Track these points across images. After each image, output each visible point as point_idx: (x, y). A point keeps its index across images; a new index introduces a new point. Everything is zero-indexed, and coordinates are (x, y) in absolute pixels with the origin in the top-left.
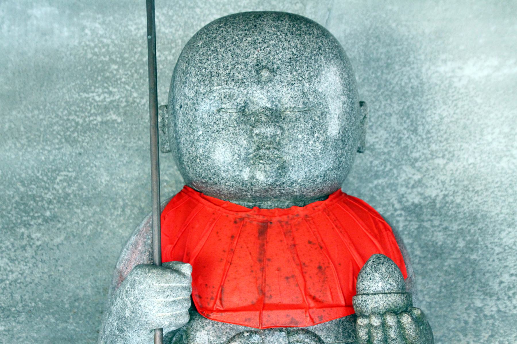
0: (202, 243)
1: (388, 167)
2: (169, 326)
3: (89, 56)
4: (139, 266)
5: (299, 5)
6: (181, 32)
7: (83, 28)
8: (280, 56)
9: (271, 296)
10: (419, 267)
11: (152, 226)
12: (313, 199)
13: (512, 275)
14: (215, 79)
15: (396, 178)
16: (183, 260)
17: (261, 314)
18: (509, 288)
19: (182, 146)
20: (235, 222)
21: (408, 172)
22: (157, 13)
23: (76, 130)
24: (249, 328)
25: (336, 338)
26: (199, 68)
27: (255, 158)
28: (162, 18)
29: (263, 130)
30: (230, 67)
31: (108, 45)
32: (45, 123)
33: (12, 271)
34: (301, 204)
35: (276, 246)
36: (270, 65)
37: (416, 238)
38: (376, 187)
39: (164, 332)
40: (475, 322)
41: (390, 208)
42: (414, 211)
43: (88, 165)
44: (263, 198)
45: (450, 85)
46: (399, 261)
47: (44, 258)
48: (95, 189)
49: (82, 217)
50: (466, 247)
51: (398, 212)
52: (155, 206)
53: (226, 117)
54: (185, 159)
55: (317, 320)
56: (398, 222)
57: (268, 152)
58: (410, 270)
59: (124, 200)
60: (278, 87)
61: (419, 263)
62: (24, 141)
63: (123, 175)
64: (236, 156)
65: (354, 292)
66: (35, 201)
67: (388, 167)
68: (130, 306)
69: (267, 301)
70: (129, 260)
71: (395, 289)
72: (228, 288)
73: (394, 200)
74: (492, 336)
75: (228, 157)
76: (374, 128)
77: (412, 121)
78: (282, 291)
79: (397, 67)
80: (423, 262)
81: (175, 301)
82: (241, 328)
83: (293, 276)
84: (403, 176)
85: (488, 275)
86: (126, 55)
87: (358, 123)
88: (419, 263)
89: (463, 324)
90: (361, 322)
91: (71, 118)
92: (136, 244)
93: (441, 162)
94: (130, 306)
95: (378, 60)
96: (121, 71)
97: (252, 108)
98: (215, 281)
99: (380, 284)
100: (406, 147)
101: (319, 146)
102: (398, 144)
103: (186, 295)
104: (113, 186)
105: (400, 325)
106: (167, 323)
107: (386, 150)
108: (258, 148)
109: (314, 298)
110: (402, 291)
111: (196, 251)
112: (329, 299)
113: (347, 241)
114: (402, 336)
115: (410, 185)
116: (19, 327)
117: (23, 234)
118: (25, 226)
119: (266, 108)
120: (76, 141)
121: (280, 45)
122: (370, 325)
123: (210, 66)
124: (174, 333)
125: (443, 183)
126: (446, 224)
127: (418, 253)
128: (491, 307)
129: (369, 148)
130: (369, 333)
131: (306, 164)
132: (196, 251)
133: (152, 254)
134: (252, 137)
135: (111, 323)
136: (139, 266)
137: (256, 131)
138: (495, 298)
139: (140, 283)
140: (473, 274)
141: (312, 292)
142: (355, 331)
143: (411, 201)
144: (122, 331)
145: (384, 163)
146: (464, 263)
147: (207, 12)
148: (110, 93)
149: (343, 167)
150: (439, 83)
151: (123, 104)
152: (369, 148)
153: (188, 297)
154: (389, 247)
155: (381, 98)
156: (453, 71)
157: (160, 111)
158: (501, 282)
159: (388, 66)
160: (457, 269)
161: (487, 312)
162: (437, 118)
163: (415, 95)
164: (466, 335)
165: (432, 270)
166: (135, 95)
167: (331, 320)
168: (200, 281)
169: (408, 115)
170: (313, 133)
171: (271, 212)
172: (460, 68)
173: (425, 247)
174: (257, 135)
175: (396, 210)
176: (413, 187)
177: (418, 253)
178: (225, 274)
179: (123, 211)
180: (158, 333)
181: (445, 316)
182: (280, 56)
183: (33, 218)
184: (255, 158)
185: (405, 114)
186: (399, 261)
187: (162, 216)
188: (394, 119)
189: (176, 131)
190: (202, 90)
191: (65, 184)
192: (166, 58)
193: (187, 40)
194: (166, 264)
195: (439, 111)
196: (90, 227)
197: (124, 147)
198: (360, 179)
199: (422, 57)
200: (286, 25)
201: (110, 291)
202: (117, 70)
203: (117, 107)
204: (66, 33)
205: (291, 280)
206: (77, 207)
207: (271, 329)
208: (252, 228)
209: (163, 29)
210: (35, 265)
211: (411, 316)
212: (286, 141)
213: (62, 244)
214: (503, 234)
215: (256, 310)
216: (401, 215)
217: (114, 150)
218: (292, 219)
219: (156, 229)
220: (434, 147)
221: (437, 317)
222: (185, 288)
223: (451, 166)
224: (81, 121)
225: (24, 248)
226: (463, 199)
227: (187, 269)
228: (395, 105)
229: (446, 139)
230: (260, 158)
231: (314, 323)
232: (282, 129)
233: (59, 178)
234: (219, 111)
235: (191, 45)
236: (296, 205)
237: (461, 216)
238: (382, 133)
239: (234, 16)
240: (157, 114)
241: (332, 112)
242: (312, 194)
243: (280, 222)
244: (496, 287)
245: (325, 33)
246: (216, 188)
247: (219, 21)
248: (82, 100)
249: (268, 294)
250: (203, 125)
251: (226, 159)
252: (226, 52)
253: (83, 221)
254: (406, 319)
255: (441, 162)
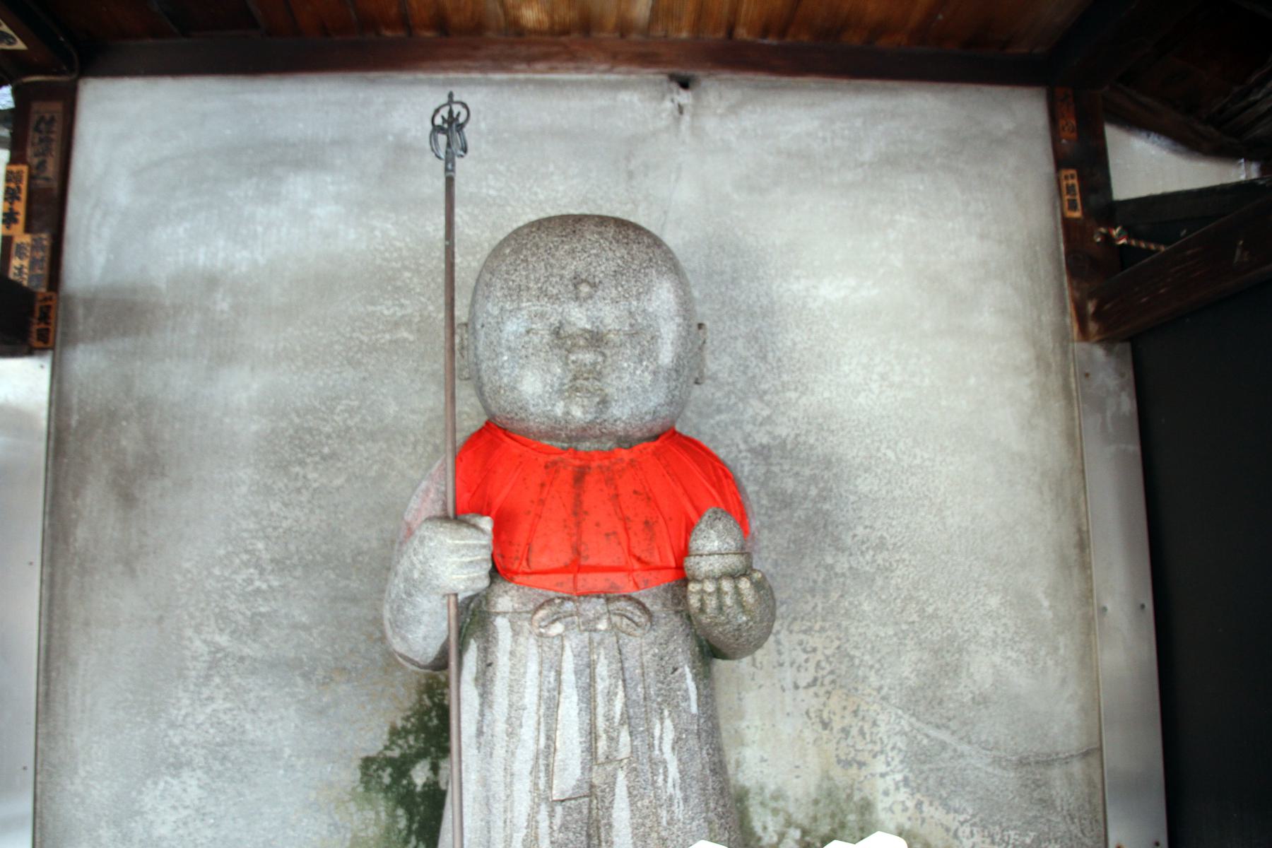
0: (506, 491)
1: (733, 400)
2: (466, 590)
3: (378, 261)
4: (430, 519)
5: (629, 206)
6: (487, 234)
7: (373, 229)
8: (603, 268)
9: (587, 557)
10: (765, 519)
11: (445, 469)
12: (640, 440)
13: (866, 527)
14: (524, 293)
15: (742, 414)
16: (482, 513)
17: (575, 578)
18: (863, 542)
19: (482, 373)
20: (546, 467)
21: (755, 408)
22: (458, 210)
23: (360, 350)
24: (560, 594)
25: (664, 605)
26: (506, 280)
27: (571, 389)
28: (466, 218)
29: (581, 356)
30: (542, 280)
31: (400, 249)
32: (324, 341)
33: (286, 518)
34: (626, 446)
35: (595, 495)
36: (590, 279)
37: (764, 484)
38: (718, 424)
39: (460, 597)
40: (825, 581)
41: (734, 449)
42: (763, 453)
43: (373, 393)
44: (579, 438)
45: (804, 307)
46: (741, 516)
47: (323, 502)
48: (381, 421)
49: (366, 455)
50: (819, 495)
51: (744, 454)
52: (450, 446)
53: (536, 340)
54: (487, 389)
55: (642, 585)
56: (742, 466)
57: (586, 383)
58: (754, 524)
59: (415, 435)
60: (600, 305)
61: (766, 514)
62: (300, 363)
63: (416, 409)
64: (548, 388)
65: (684, 552)
66: (312, 435)
67: (733, 400)
68: (419, 566)
69: (583, 562)
70: (418, 510)
71: (733, 550)
72: (536, 547)
73: (738, 438)
74: (842, 596)
75: (538, 388)
76: (717, 354)
77: (761, 347)
78: (601, 550)
79: (744, 282)
80: (770, 512)
81: (471, 562)
82: (552, 594)
83: (615, 533)
84: (750, 412)
85: (841, 527)
86: (422, 261)
87: (696, 350)
88: (766, 514)
89: (811, 584)
90: (693, 587)
91: (355, 335)
92: (427, 491)
93: (793, 395)
94: (419, 566)
95: (722, 273)
96: (415, 280)
97: (569, 330)
98: (521, 536)
99: (716, 544)
100: (754, 377)
101: (648, 377)
102: (744, 373)
103: (485, 554)
104: (403, 418)
105: (737, 591)
106: (462, 587)
107: (730, 380)
108: (575, 378)
109: (639, 559)
110: (743, 552)
111: (498, 502)
112: (656, 560)
113: (680, 491)
114: (740, 602)
115: (758, 423)
116: (295, 583)
117: (297, 474)
118: (300, 464)
119: (585, 330)
120: (359, 363)
121: (603, 255)
122: (702, 591)
123: (518, 278)
124: (471, 598)
125: (795, 420)
126: (797, 469)
127: (764, 502)
128: (843, 564)
129: (710, 378)
130: (702, 601)
131: (633, 398)
132: (498, 502)
133: (445, 504)
134: (567, 364)
135: (397, 585)
136: (430, 519)
137: (573, 358)
138: (847, 553)
139: (431, 539)
140: (825, 526)
141: (637, 552)
142: (685, 597)
143: (758, 441)
144: (409, 595)
145: (728, 395)
146: (816, 514)
147: (520, 211)
148: (402, 306)
149: (678, 403)
150: (791, 302)
151: (417, 320)
152: (710, 378)
153: (489, 557)
154: (729, 498)
155: (725, 318)
156: (807, 290)
157: (458, 331)
158: (855, 536)
159: (734, 281)
160: (808, 521)
161: (838, 570)
162: (789, 344)
163: (764, 316)
164: (814, 596)
165: (779, 523)
166: (431, 308)
167: (658, 584)
168: (504, 537)
169: (756, 339)
170: (641, 361)
171: (589, 456)
172: (815, 287)
173: (772, 495)
174: (573, 362)
175: (740, 452)
176: (761, 424)
177: (764, 502)
178: (533, 530)
179: (415, 448)
180: (452, 599)
181: (792, 575)
182: (603, 268)
183: (310, 455)
184: (571, 389)
185: (753, 338)
186: (741, 516)
187: (458, 459)
188: (740, 344)
189: (476, 356)
190: (508, 306)
191: (346, 415)
192: (467, 265)
193: (495, 243)
194: (461, 517)
195: (791, 336)
196: (375, 467)
197: (416, 371)
198: (700, 414)
199: (773, 272)
200: (611, 231)
201: (396, 546)
202: (411, 279)
203: (410, 323)
204: (352, 235)
205: (612, 537)
206: (360, 443)
207: (587, 595)
208: (566, 475)
209: (467, 231)
210: (312, 511)
211: (751, 580)
212: (608, 370)
213: (342, 487)
214: (859, 481)
215: (569, 572)
216: (746, 458)
217: (405, 374)
218: (615, 464)
219: (450, 475)
220: (785, 377)
221: (783, 576)
222: (484, 547)
223: (804, 400)
224: (366, 339)
225: (298, 491)
226: (817, 440)
227: (486, 523)
228: (742, 327)
229: (800, 369)
230: (577, 390)
231: (637, 587)
232: (604, 355)
233: (340, 408)
234: (528, 332)
235: (496, 252)
236: (620, 447)
237: (814, 459)
238: (727, 360)
239: (550, 219)
240: (453, 334)
241: (665, 336)
242: (639, 434)
243: (600, 467)
244: (849, 541)
245: (657, 242)
246: (523, 425)
247: (531, 225)
248: (368, 314)
249: (584, 554)
250: (509, 349)
251: (535, 391)
252: (538, 261)
253: (367, 459)
254: (744, 584)
255: (793, 395)
